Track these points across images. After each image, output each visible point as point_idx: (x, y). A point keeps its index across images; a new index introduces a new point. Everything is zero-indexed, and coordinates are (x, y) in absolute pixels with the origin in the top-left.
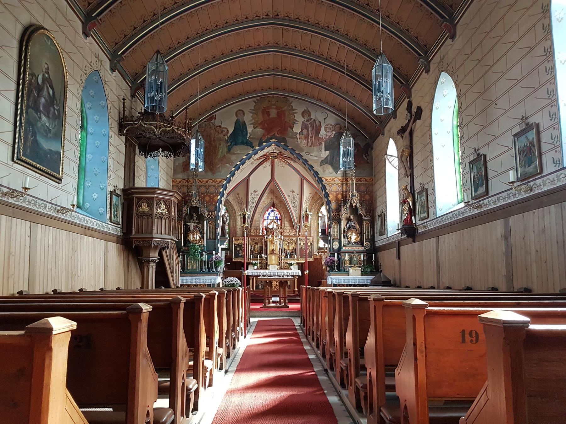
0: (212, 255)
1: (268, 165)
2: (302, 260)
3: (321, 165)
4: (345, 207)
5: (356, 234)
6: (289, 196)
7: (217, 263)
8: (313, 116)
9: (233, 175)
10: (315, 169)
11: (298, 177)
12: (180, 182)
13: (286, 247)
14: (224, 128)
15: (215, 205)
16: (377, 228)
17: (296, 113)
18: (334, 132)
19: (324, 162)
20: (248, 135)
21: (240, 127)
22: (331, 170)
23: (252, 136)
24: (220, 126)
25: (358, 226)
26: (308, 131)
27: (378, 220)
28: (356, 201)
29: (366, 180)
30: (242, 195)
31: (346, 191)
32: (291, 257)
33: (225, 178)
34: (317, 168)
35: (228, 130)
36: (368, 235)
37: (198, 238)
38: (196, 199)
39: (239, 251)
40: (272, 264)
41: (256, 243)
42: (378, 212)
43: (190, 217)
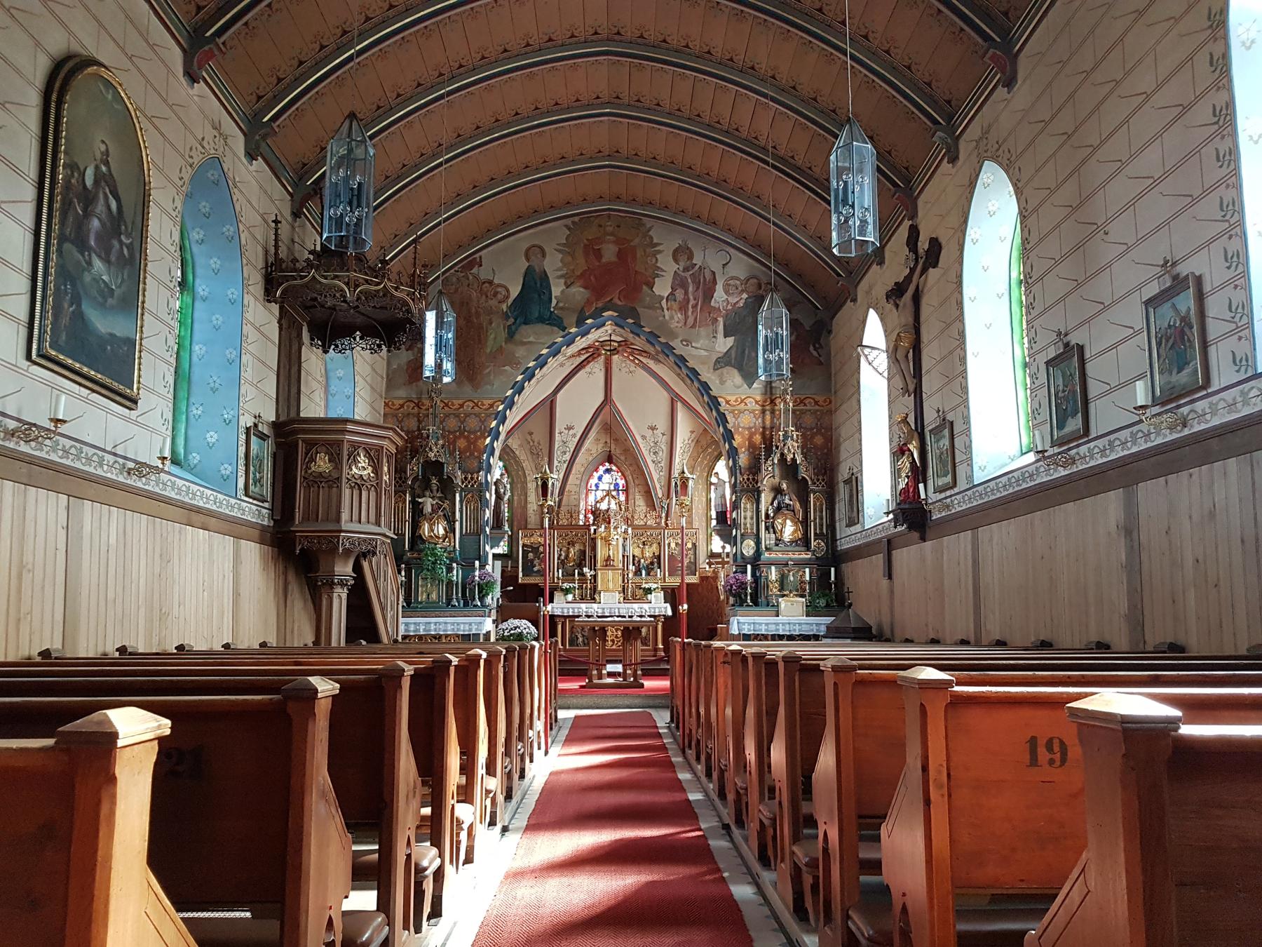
0: (474, 570)
1: (597, 368)
2: (674, 581)
3: (715, 370)
4: (769, 462)
5: (795, 523)
6: (644, 437)
7: (484, 588)
8: (697, 260)
9: (520, 390)
10: (703, 378)
11: (664, 396)
12: (402, 406)
13: (637, 552)
14: (499, 285)
15: (479, 458)
16: (841, 509)
17: (660, 252)
18: (745, 296)
19: (722, 362)
20: (554, 302)
21: (535, 284)
22: (738, 379)
23: (561, 305)
24: (491, 282)
25: (798, 505)
26: (686, 293)
27: (842, 492)
28: (793, 449)
30: (540, 436)
31: (772, 428)
32: (648, 574)
33: (502, 396)
34: (707, 375)
35: (508, 291)
36: (821, 525)
37: (442, 532)
38: (436, 444)
39: (532, 561)
40: (607, 590)
41: (571, 543)
42: (843, 473)
43: (424, 485)
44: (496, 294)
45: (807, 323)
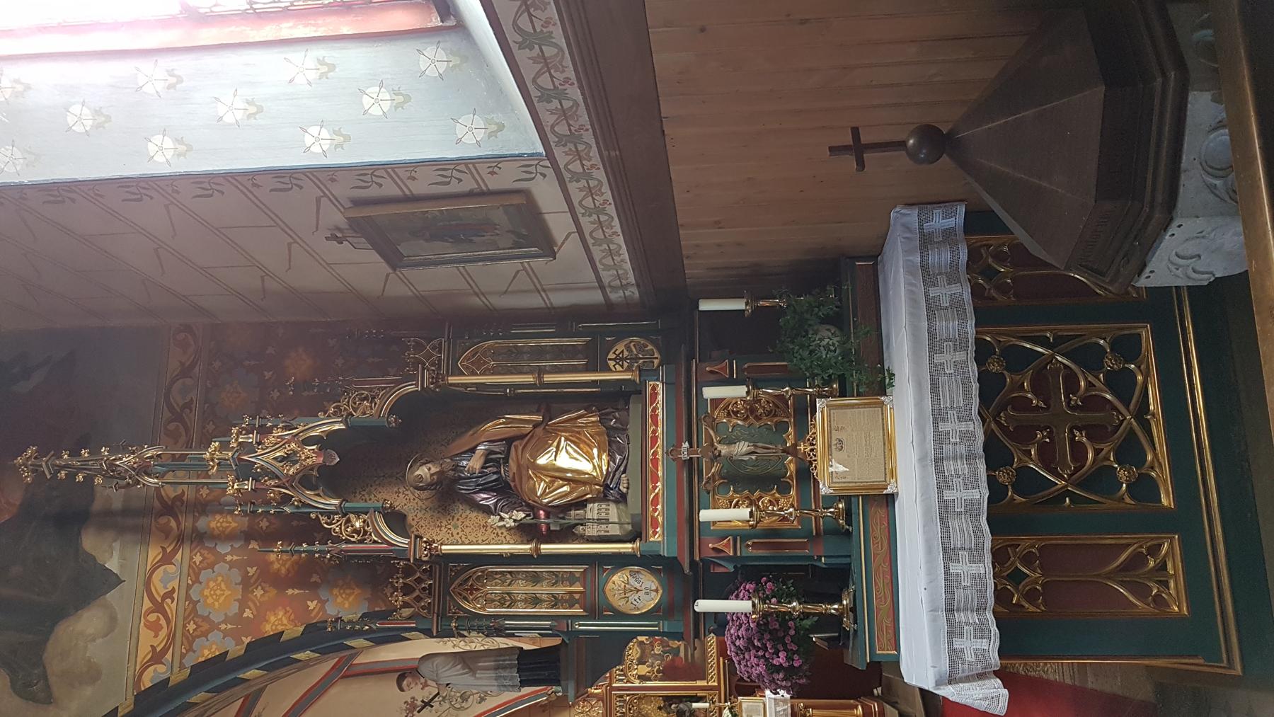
5: (542, 438)
16: (500, 281)
22: (89, 622)
25: (494, 428)
26: (185, 626)
27: (438, 279)
28: (288, 446)
29: (186, 372)
36: (560, 352)
42: (362, 269)
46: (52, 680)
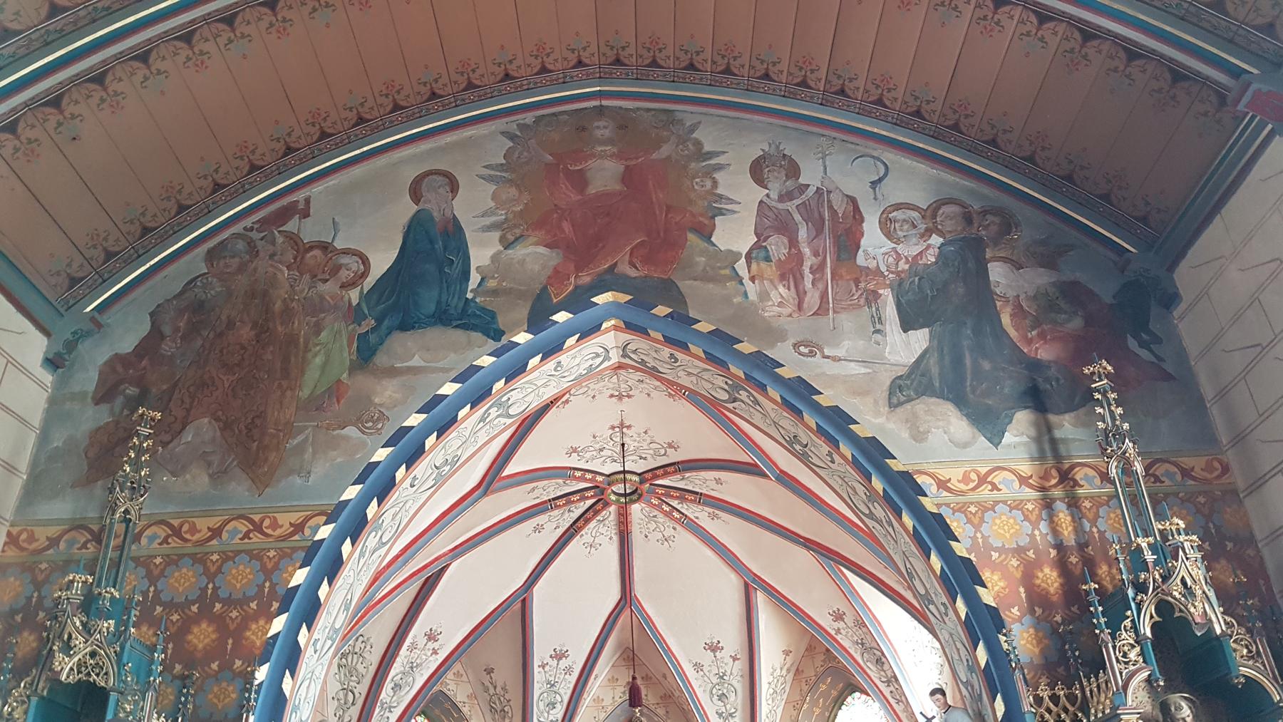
1: (602, 532)
3: (893, 406)
4: (1126, 637)
6: (698, 667)
8: (811, 176)
9: (384, 489)
10: (861, 430)
11: (731, 584)
12: (53, 542)
14: (346, 252)
17: (720, 167)
18: (936, 240)
19: (908, 387)
20: (475, 279)
21: (432, 249)
23: (492, 284)
24: (325, 247)
26: (793, 243)
30: (506, 674)
31: (1082, 546)
33: (330, 502)
34: (872, 420)
35: (365, 261)
44: (338, 268)
45: (1106, 291)
46: (908, 406)
